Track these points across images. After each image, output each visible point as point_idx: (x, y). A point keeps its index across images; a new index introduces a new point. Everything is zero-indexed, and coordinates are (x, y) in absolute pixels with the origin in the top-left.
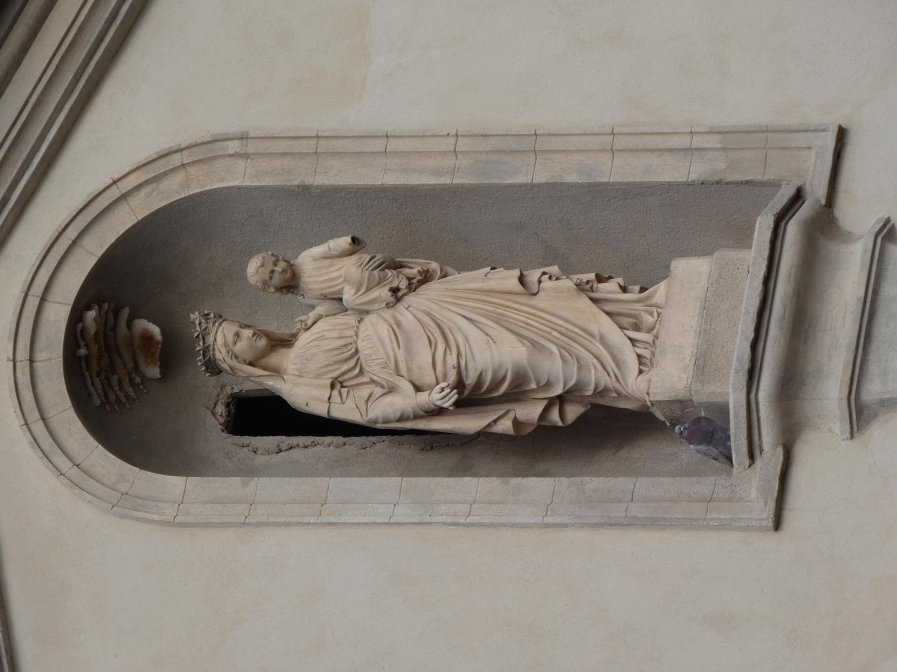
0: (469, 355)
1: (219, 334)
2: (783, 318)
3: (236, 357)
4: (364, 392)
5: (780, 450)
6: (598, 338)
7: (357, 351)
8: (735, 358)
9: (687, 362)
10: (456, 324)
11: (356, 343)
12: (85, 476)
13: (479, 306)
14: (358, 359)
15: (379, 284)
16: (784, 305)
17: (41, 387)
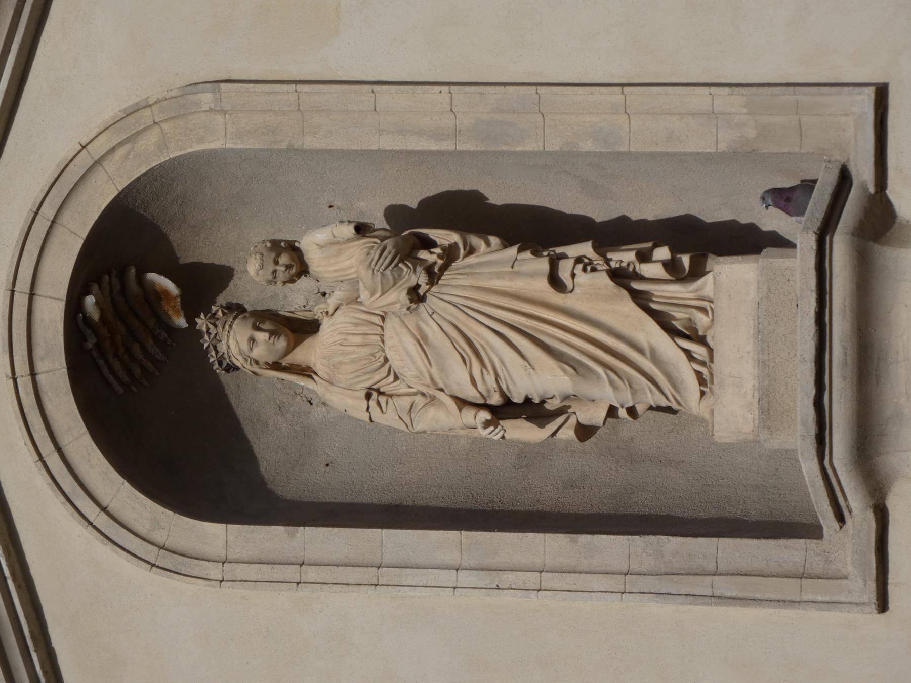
0: (508, 379)
1: (231, 340)
2: (845, 364)
3: (257, 362)
4: (406, 402)
5: (870, 515)
6: (648, 353)
7: (386, 360)
8: (799, 418)
9: (749, 396)
10: (487, 342)
11: (383, 351)
12: (116, 524)
14: (390, 368)
15: (395, 284)
16: (844, 348)
17: (49, 407)
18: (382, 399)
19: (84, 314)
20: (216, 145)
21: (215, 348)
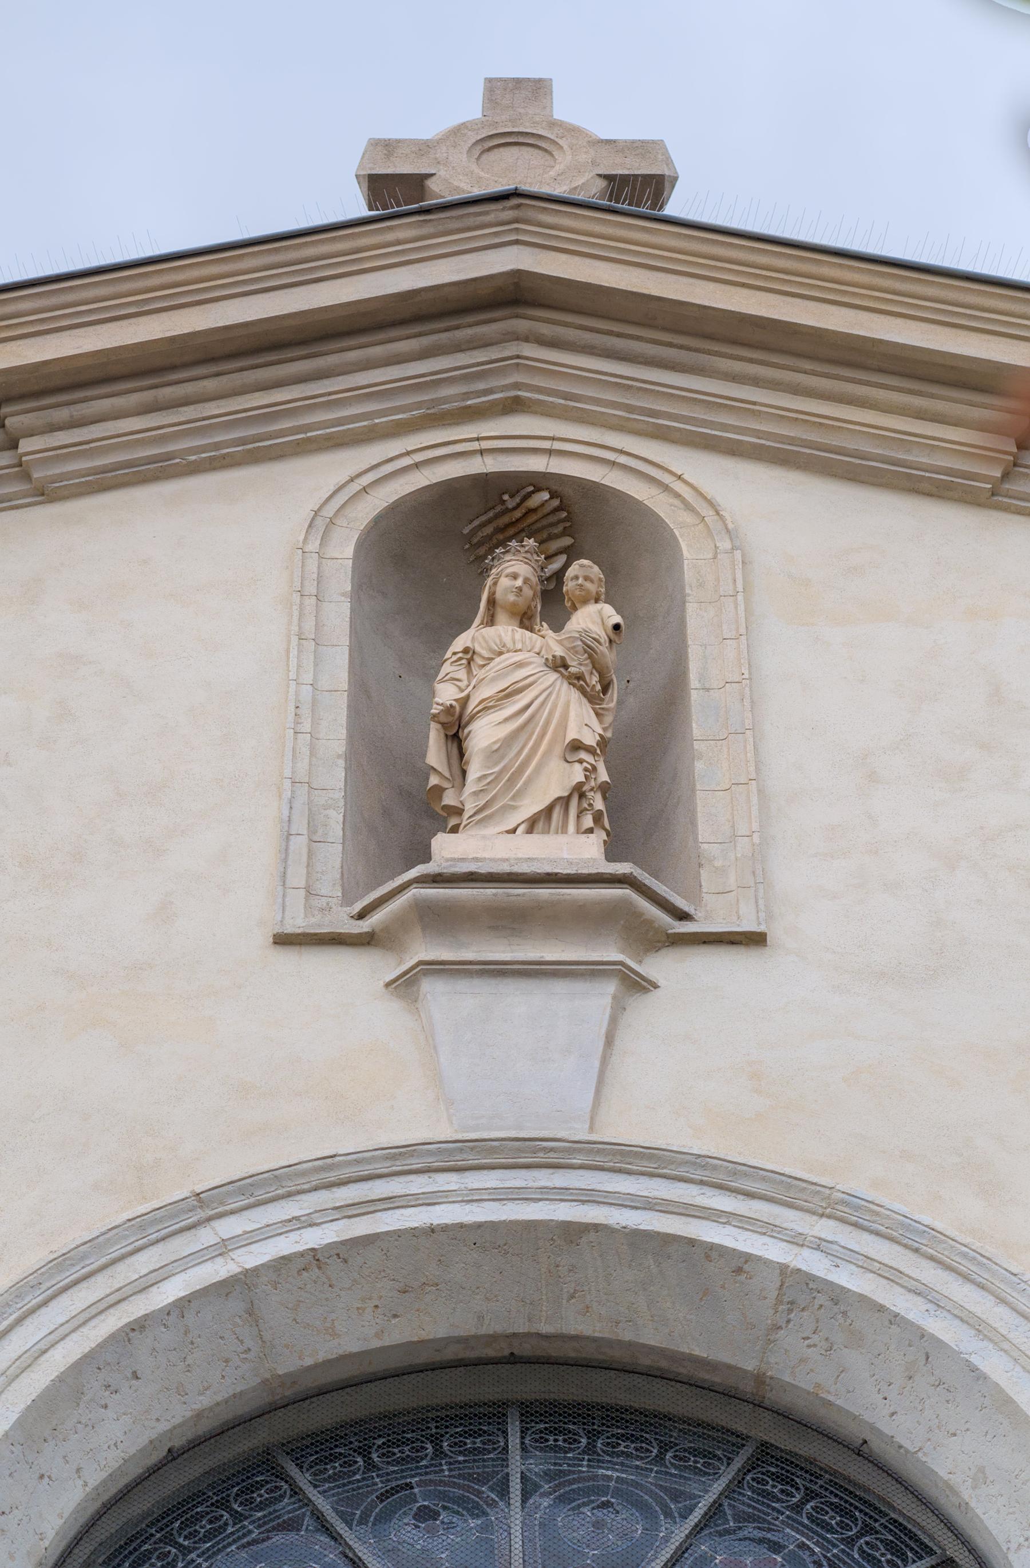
13: (214, 270)
18: (464, 661)
19: (533, 492)
20: (686, 553)
21: (507, 552)
